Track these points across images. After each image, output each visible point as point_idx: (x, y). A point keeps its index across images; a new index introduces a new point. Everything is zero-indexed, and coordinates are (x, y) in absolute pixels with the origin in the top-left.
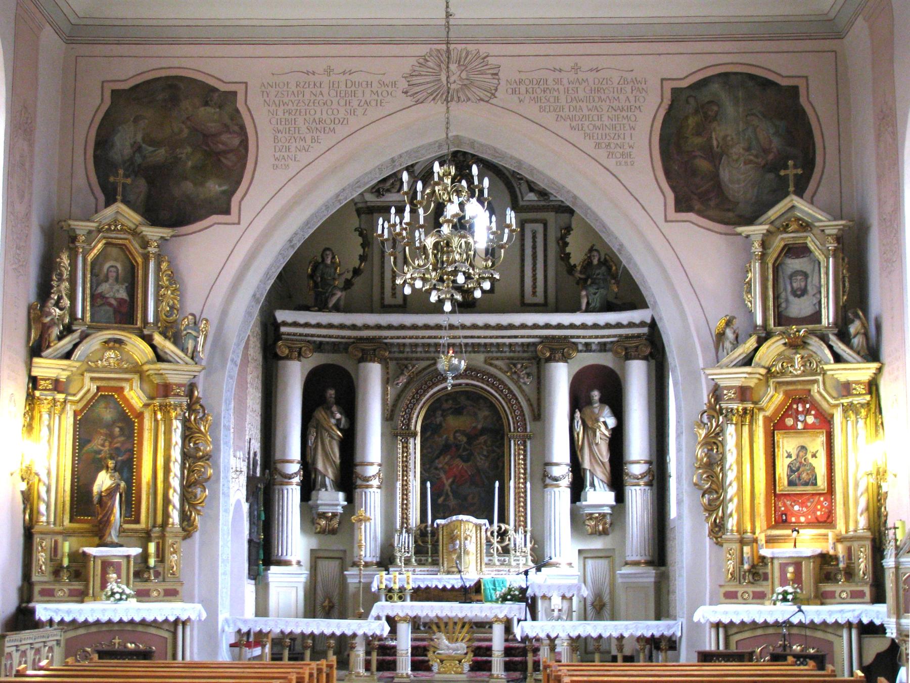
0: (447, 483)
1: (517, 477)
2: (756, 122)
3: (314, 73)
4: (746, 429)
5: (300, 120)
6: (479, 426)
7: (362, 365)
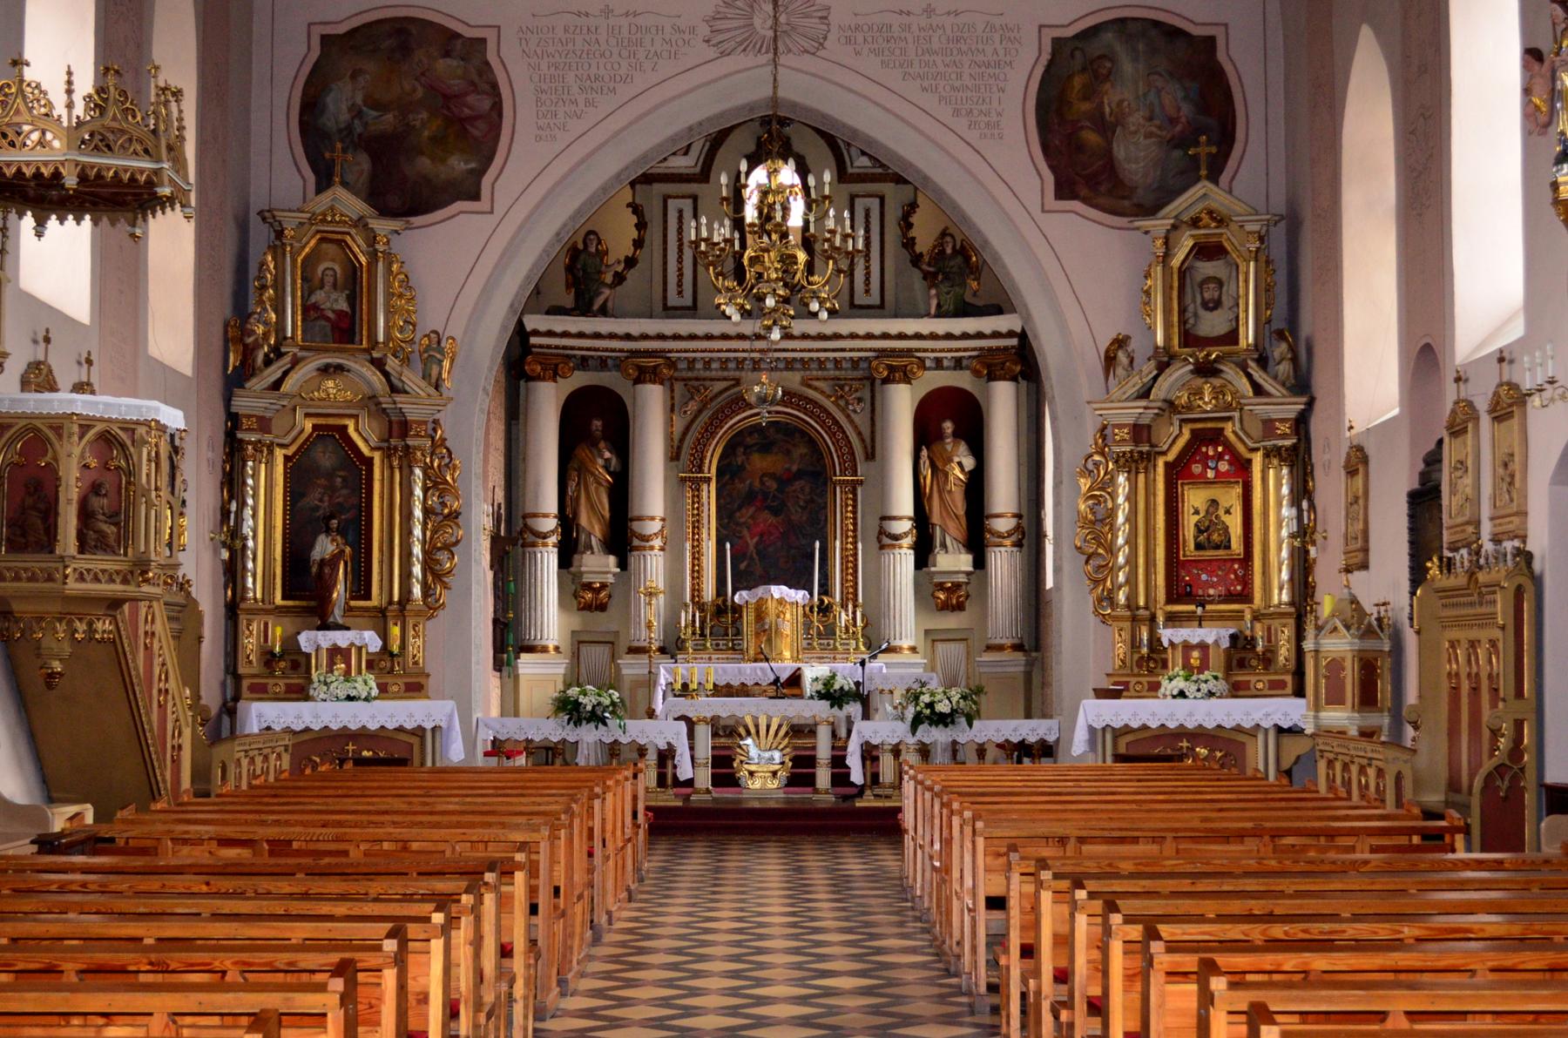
0: (752, 542)
1: (845, 536)
2: (1160, 83)
3: (587, 15)
4: (1141, 477)
5: (570, 77)
6: (795, 468)
7: (639, 386)
